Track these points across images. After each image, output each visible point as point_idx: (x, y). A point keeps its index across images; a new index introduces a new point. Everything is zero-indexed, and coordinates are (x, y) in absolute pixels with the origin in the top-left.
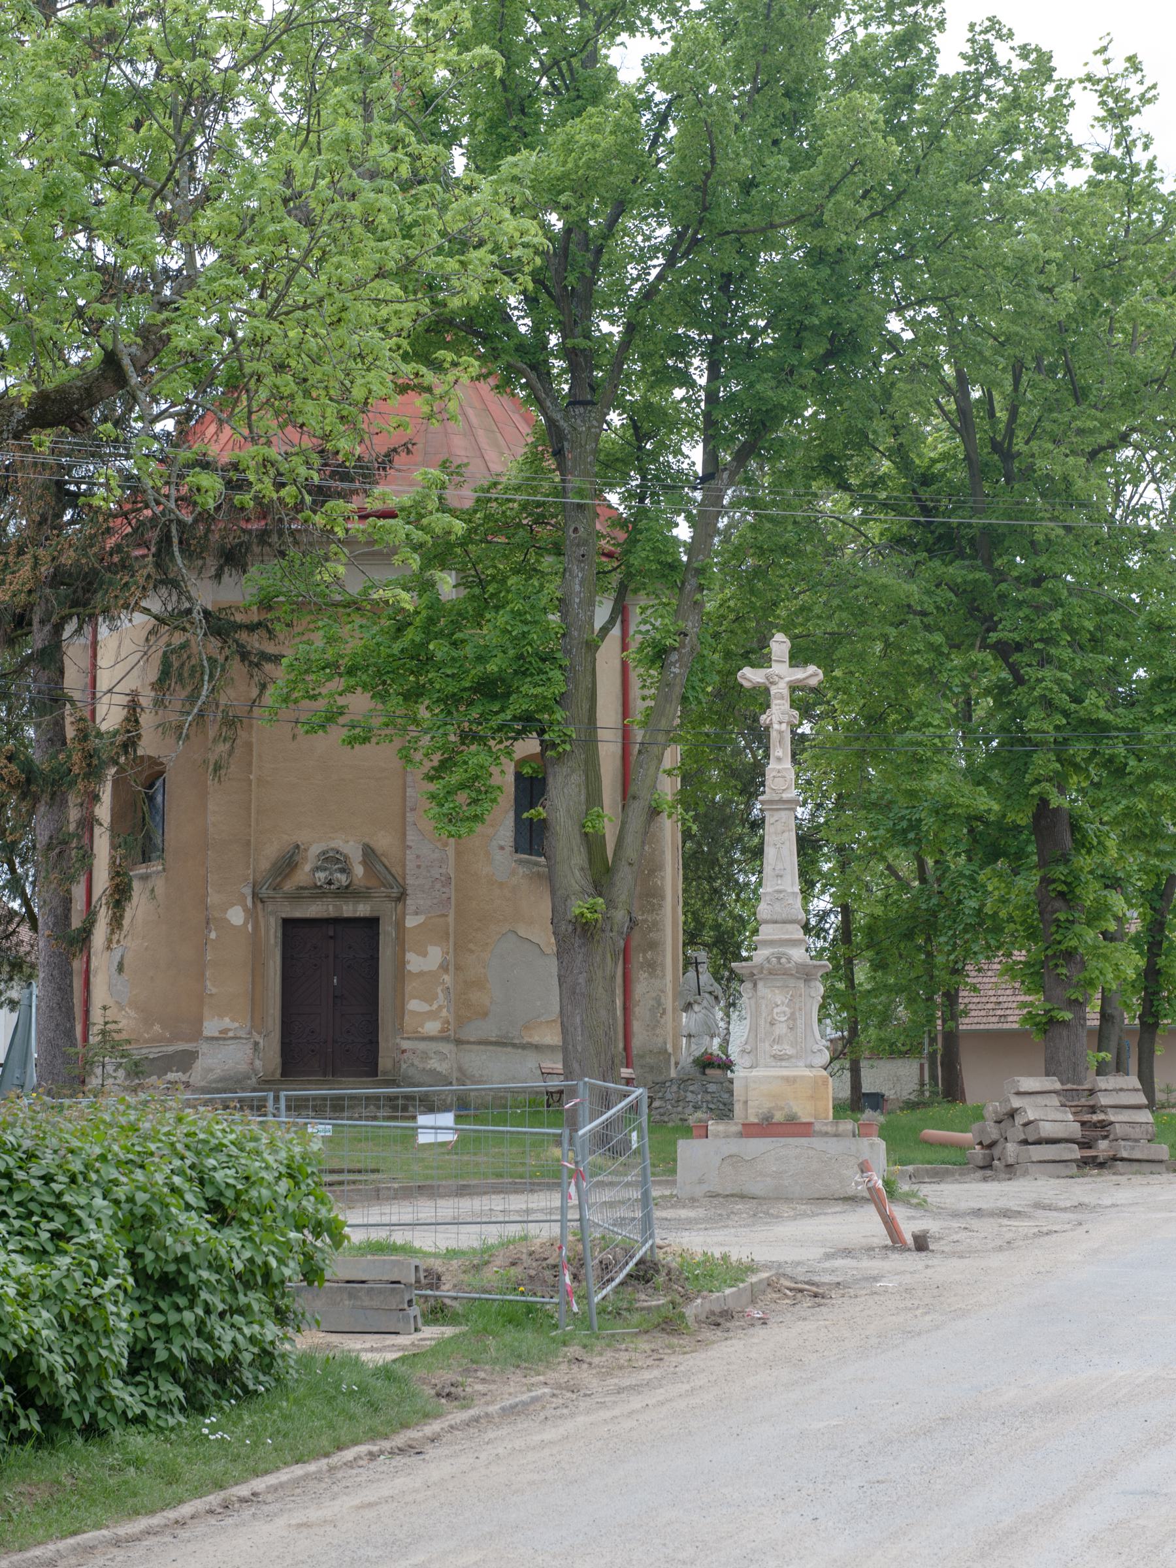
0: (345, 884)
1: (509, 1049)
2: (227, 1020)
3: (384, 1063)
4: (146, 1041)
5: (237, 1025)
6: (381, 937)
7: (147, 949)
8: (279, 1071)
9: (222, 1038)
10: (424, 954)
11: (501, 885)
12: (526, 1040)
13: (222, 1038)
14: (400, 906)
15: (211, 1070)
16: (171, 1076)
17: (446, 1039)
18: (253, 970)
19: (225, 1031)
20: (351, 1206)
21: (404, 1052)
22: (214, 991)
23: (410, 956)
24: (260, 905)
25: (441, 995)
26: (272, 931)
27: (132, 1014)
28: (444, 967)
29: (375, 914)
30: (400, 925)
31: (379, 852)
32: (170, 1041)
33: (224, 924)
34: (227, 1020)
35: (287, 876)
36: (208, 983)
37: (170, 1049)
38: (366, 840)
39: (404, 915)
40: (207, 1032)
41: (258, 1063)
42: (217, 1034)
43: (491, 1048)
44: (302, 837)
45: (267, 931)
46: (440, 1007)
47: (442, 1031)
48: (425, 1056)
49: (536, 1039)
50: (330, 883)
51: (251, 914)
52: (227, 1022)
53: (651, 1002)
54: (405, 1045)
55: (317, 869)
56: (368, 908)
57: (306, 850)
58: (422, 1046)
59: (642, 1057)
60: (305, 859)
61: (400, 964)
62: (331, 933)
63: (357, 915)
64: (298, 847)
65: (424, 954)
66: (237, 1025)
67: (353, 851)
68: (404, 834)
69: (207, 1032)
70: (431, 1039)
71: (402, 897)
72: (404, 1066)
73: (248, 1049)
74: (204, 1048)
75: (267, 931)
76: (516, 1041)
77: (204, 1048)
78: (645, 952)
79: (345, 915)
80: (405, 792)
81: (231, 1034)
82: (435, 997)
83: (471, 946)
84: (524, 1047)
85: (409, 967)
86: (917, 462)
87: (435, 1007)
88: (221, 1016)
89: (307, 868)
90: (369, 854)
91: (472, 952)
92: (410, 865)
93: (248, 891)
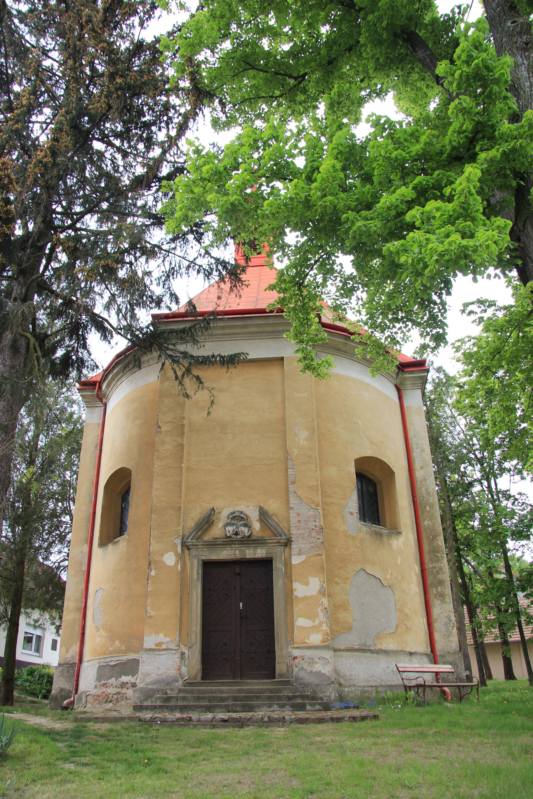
0: (247, 535)
1: (368, 654)
2: (161, 635)
3: (280, 667)
4: (110, 653)
5: (168, 639)
6: (274, 572)
7: (114, 588)
8: (200, 676)
9: (156, 650)
10: (307, 584)
11: (353, 538)
12: (378, 647)
13: (156, 650)
14: (287, 550)
15: (149, 675)
16: (124, 679)
17: (327, 647)
18: (181, 598)
19: (159, 644)
20: (325, 105)
21: (295, 658)
22: (153, 613)
23: (296, 585)
24: (187, 552)
25: (321, 614)
26: (195, 570)
27: (103, 633)
28: (322, 592)
29: (269, 556)
30: (287, 563)
31: (271, 513)
32: (125, 652)
33: (161, 565)
34: (161, 635)
35: (207, 530)
36: (148, 608)
37: (125, 658)
38: (262, 505)
39: (290, 555)
40: (146, 645)
41: (184, 669)
42: (153, 647)
43: (356, 653)
44: (216, 504)
45: (192, 569)
46: (321, 623)
47: (323, 641)
48: (312, 661)
49: (384, 647)
50: (236, 534)
51: (181, 558)
52: (161, 638)
53: (445, 620)
54: (296, 653)
55: (227, 525)
56: (264, 551)
57: (219, 513)
58: (308, 653)
59: (443, 656)
60: (219, 519)
61: (289, 592)
62: (238, 571)
63: (257, 556)
64: (213, 509)
65: (307, 584)
66: (168, 639)
67: (254, 515)
68: (288, 501)
69: (146, 645)
70: (315, 647)
71: (288, 543)
72: (296, 670)
73: (176, 658)
74: (143, 657)
75: (192, 569)
76: (372, 648)
77: (143, 657)
78: (436, 587)
79: (248, 557)
80: (287, 472)
81: (164, 646)
82: (317, 615)
83: (337, 579)
84: (379, 652)
85: (295, 593)
86: (450, 439)
87: (317, 622)
88: (157, 633)
89: (220, 525)
90: (263, 515)
91: (338, 583)
92: (293, 520)
93: (178, 542)
